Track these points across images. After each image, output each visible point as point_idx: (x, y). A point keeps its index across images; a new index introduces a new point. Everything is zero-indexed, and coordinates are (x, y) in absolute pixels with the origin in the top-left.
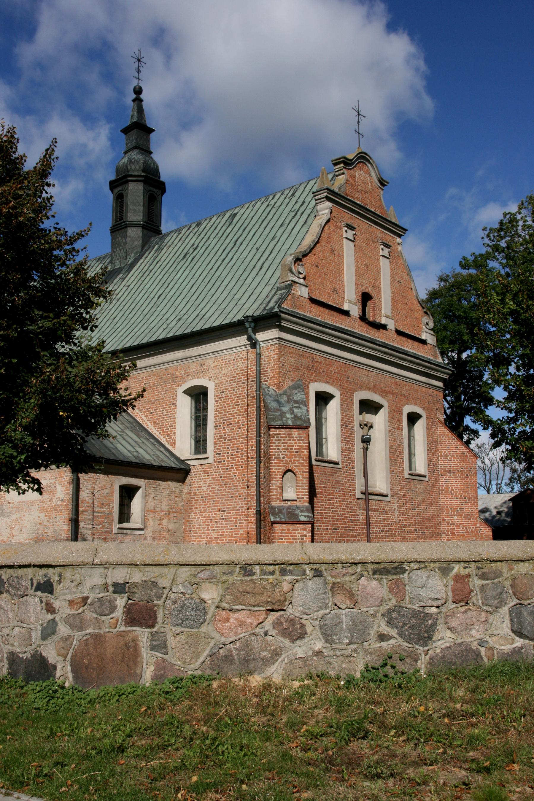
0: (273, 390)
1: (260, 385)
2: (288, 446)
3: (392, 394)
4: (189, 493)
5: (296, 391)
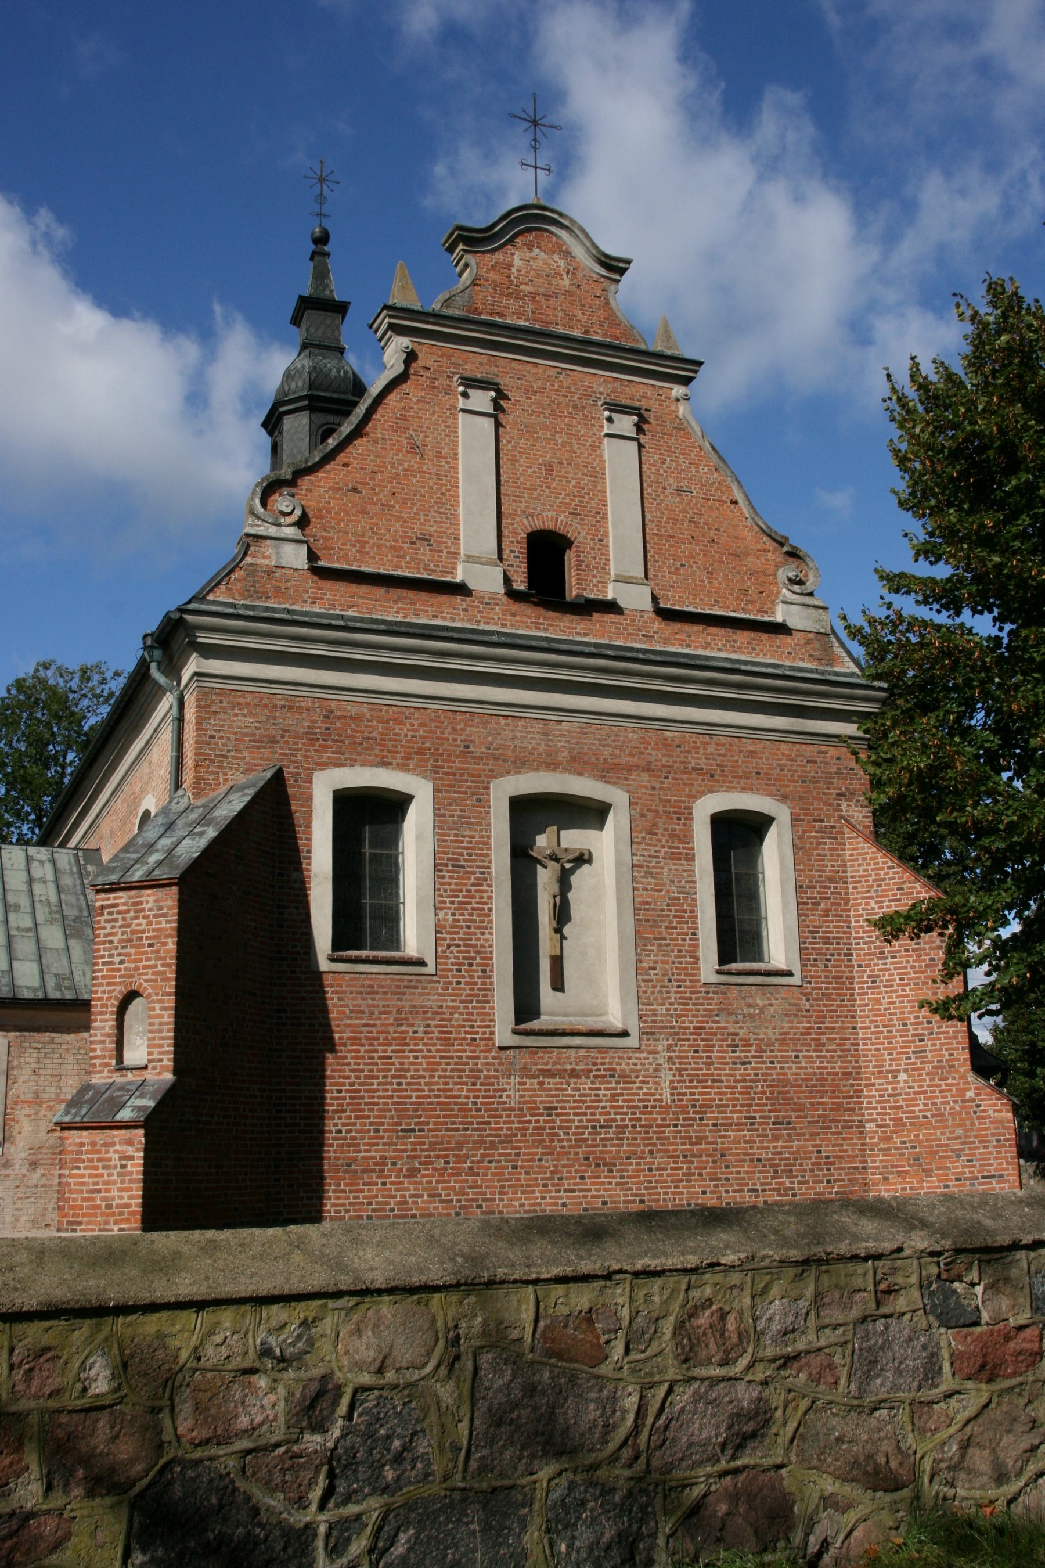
2: (133, 932)
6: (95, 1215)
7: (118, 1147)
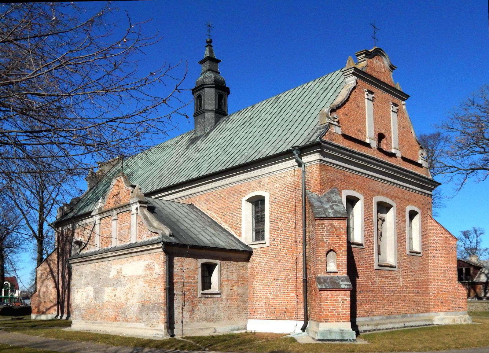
0: (315, 195)
1: (305, 192)
3: (399, 198)
4: (252, 267)
5: (333, 195)
6: (334, 317)
7: (341, 296)
